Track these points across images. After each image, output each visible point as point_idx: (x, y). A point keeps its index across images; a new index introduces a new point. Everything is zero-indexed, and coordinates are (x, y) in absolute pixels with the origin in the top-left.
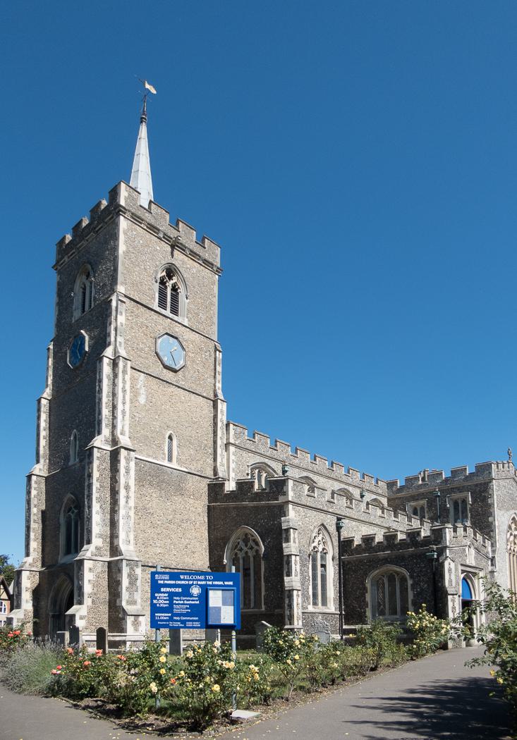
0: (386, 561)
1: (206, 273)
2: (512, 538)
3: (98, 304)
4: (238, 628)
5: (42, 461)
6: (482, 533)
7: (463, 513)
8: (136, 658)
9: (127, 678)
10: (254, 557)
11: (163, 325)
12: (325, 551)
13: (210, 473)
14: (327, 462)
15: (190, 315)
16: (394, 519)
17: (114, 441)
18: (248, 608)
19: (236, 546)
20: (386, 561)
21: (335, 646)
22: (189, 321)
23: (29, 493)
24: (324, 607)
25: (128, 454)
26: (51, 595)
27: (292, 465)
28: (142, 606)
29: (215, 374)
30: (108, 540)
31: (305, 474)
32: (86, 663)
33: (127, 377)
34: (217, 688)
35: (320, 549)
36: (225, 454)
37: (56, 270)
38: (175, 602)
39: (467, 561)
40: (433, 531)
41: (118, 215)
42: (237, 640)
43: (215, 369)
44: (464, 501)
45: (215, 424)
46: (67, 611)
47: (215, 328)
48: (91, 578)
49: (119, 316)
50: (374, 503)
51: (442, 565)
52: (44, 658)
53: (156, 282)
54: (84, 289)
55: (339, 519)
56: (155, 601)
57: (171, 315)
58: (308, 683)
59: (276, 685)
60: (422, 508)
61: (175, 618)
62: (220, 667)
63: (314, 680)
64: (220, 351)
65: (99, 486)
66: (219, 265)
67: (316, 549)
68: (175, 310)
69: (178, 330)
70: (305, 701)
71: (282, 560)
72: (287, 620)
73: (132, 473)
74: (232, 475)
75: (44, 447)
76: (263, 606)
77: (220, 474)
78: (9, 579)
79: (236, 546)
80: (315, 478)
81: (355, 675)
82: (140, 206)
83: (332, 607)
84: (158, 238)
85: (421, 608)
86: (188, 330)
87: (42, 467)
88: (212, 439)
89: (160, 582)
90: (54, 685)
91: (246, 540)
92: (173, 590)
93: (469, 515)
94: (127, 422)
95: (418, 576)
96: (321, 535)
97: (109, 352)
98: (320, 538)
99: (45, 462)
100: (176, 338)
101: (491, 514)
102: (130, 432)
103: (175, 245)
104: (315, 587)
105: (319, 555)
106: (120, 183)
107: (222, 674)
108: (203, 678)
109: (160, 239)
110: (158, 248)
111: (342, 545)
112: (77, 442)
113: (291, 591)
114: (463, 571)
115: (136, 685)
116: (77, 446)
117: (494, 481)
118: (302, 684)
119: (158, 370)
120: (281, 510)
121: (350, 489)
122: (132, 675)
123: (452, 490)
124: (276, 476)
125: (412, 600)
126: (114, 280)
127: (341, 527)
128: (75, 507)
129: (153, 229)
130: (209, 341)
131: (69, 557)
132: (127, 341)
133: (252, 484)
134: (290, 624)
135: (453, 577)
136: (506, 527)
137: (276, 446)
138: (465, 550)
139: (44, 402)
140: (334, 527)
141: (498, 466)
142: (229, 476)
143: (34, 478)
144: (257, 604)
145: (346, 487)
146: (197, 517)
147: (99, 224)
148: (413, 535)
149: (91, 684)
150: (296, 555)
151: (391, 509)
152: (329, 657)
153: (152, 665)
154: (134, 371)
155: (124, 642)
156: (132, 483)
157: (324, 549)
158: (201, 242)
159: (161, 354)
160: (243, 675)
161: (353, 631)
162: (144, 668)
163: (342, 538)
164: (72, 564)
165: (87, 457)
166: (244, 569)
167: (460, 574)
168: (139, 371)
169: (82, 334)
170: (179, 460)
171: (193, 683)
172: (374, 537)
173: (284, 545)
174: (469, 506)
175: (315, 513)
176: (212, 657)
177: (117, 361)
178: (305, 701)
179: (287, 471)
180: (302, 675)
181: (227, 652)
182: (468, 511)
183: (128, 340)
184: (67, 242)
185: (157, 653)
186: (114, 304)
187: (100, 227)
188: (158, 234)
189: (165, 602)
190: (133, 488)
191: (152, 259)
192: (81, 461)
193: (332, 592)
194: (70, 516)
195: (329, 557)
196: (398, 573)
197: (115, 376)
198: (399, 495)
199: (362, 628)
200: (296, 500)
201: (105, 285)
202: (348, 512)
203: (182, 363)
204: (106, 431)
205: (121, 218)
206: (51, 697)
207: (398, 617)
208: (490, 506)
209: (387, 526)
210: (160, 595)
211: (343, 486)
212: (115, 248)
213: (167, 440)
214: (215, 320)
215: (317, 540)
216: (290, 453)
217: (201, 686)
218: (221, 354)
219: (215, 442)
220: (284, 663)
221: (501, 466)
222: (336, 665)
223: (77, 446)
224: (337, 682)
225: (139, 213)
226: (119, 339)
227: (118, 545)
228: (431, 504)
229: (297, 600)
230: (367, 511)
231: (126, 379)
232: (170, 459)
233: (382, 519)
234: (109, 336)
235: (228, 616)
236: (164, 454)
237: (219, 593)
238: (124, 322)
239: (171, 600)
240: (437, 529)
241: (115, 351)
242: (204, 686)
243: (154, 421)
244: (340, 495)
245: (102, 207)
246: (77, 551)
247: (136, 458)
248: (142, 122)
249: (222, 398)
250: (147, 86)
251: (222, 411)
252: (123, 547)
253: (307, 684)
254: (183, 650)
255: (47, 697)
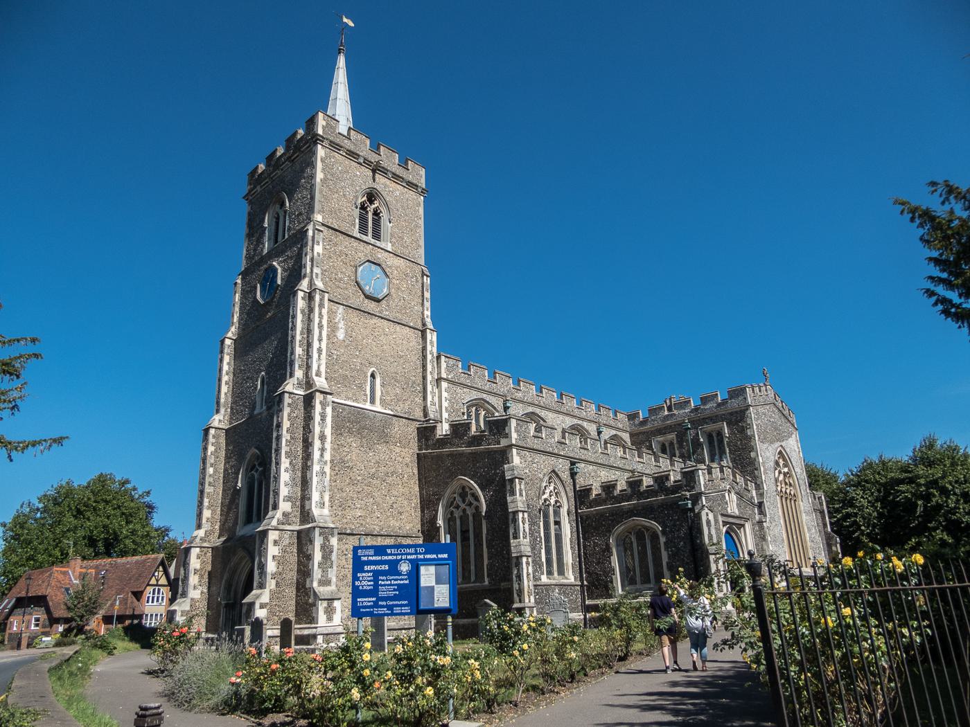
0: (632, 512)
1: (411, 194)
2: (781, 477)
3: (293, 234)
4: (455, 611)
5: (222, 410)
6: (743, 474)
7: (720, 448)
8: (334, 656)
9: (322, 684)
10: (474, 516)
11: (363, 252)
12: (558, 504)
13: (418, 414)
14: (555, 394)
15: (393, 240)
16: (638, 459)
17: (308, 383)
18: (469, 583)
19: (452, 503)
20: (632, 512)
21: (573, 629)
22: (393, 245)
23: (205, 449)
24: (561, 577)
25: (324, 398)
26: (225, 578)
27: (515, 400)
28: (337, 586)
29: (423, 301)
30: (298, 503)
31: (530, 409)
32: (274, 667)
33: (325, 311)
34: (430, 691)
35: (552, 502)
36: (436, 391)
37: (247, 200)
38: (380, 582)
39: (729, 509)
40: (684, 474)
41: (315, 143)
42: (454, 626)
43: (423, 296)
44: (720, 434)
45: (424, 357)
46: (244, 598)
47: (422, 251)
48: (277, 554)
49: (315, 246)
50: (613, 442)
51: (698, 516)
52: (218, 663)
53: (357, 207)
54: (278, 218)
55: (573, 464)
56: (357, 583)
57: (373, 241)
58: (541, 680)
59: (500, 687)
60: (671, 444)
61: (380, 603)
62: (434, 663)
63: (547, 676)
64: (427, 276)
65: (289, 438)
66: (424, 186)
67: (548, 502)
68: (377, 235)
69: (381, 256)
70: (537, 706)
71: (507, 518)
72: (515, 595)
73: (329, 420)
74: (445, 415)
75: (226, 394)
76: (486, 579)
77: (432, 416)
78: (170, 557)
79: (452, 503)
80: (543, 413)
81: (600, 667)
82: (339, 133)
83: (571, 577)
84: (358, 163)
85: (678, 573)
86: (392, 255)
87: (222, 418)
88: (421, 374)
89: (363, 558)
90: (232, 699)
91: (463, 495)
92: (378, 567)
93: (728, 451)
94: (323, 362)
95: (671, 531)
96: (552, 485)
97: (304, 284)
98: (552, 488)
99: (226, 411)
100: (379, 265)
101: (752, 449)
102: (326, 372)
103: (376, 169)
104: (548, 552)
105: (551, 509)
106: (317, 113)
107: (436, 673)
108: (414, 679)
109: (361, 164)
110: (358, 173)
111: (579, 496)
112: (265, 387)
113: (519, 558)
114: (725, 523)
115: (333, 692)
116: (265, 392)
117: (751, 408)
118: (534, 683)
119: (359, 300)
120: (503, 456)
121: (585, 424)
122: (329, 680)
123: (704, 421)
124: (497, 414)
125: (667, 563)
126: (311, 209)
127: (576, 473)
128: (260, 465)
129: (352, 155)
130: (415, 265)
131: (250, 527)
132: (323, 271)
133: (468, 426)
134: (520, 602)
135: (713, 532)
136: (772, 464)
137: (495, 378)
138: (724, 496)
139: (228, 342)
140: (568, 473)
141: (753, 390)
142: (441, 416)
143: (212, 431)
144: (479, 577)
145: (580, 422)
146: (405, 468)
147: (294, 153)
148: (661, 480)
149: (276, 695)
150: (523, 512)
151: (634, 448)
152: (565, 643)
153: (353, 664)
154: (332, 303)
155: (315, 636)
156: (328, 432)
157: (556, 502)
158: (404, 164)
159: (362, 283)
160: (460, 672)
161: (595, 608)
162: (343, 670)
163: (578, 486)
164: (252, 537)
165: (276, 404)
166: (461, 531)
167: (721, 527)
168: (337, 303)
169: (274, 266)
170: (383, 402)
171: (402, 686)
172: (616, 484)
173: (509, 499)
174: (726, 440)
175: (544, 457)
176: (424, 651)
177: (313, 294)
178: (537, 706)
179: (508, 407)
180: (534, 671)
181: (442, 646)
182: (726, 446)
183: (325, 271)
184: (260, 171)
185: (358, 649)
186: (310, 233)
187: (296, 155)
188: (357, 159)
189: (369, 583)
190: (329, 439)
191: (352, 185)
192: (269, 408)
193: (569, 558)
194: (253, 475)
195: (564, 511)
196: (647, 529)
197: (311, 310)
198: (642, 429)
199: (605, 604)
200: (520, 443)
201: (300, 214)
202: (582, 454)
203: (385, 291)
204: (299, 374)
205: (319, 146)
206: (228, 713)
207: (652, 586)
208: (750, 438)
209: (630, 469)
210: (364, 574)
211: (576, 421)
212: (313, 177)
213: (369, 378)
214: (422, 243)
215: (548, 491)
216: (512, 386)
217: (411, 690)
218: (429, 279)
219: (424, 378)
220: (510, 655)
221: (757, 389)
222: (573, 655)
223: (265, 392)
224: (577, 678)
225: (338, 141)
226: (316, 270)
227: (310, 509)
228: (681, 436)
229: (527, 569)
230: (606, 452)
231: (322, 316)
232: (373, 402)
233: (623, 461)
234: (305, 267)
235: (442, 597)
236: (366, 395)
237: (432, 569)
238: (321, 252)
239: (376, 580)
240: (688, 471)
241: (311, 283)
242: (416, 690)
243: (354, 358)
244: (572, 434)
245: (299, 137)
246: (260, 519)
247: (333, 402)
248: (340, 53)
249: (432, 327)
250: (345, 20)
251: (431, 342)
252: (316, 511)
253: (539, 682)
254: (388, 643)
255: (223, 714)
